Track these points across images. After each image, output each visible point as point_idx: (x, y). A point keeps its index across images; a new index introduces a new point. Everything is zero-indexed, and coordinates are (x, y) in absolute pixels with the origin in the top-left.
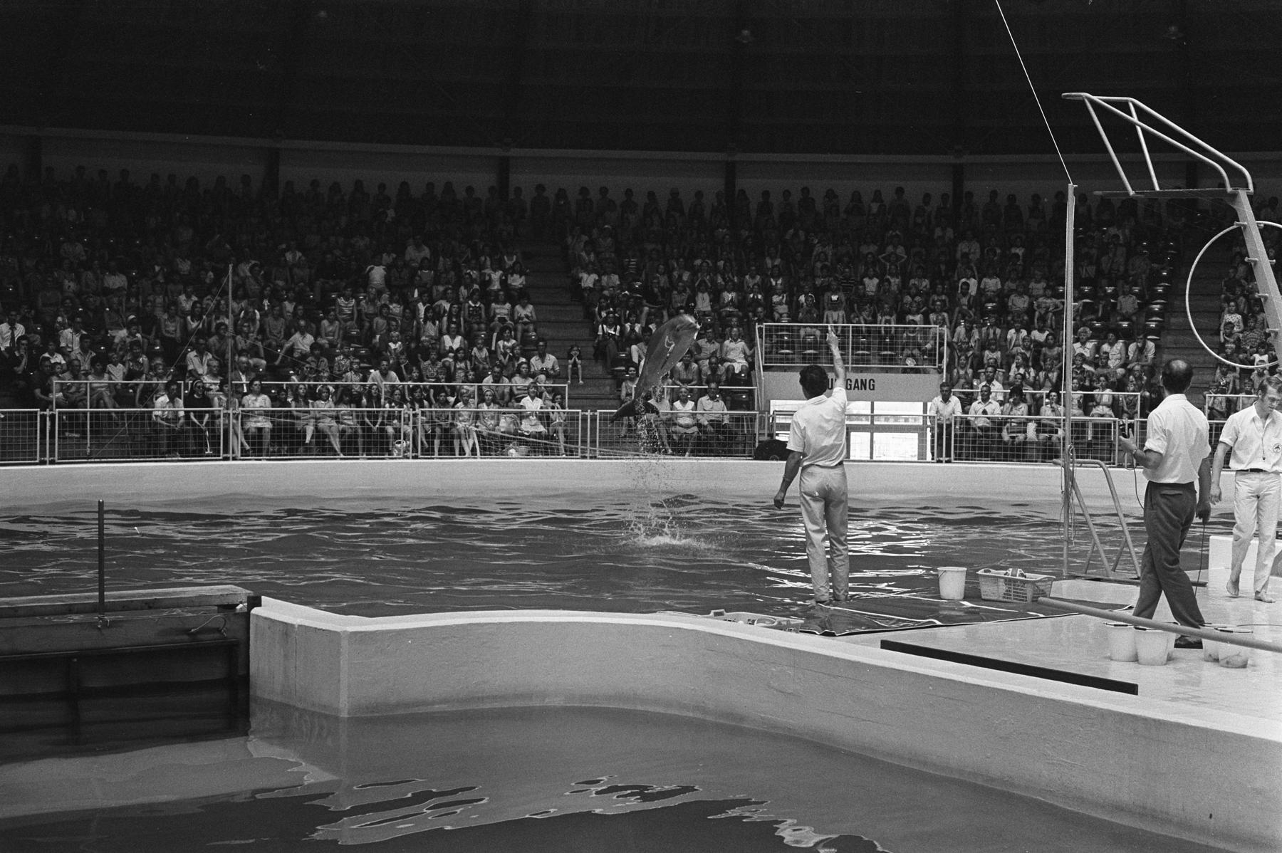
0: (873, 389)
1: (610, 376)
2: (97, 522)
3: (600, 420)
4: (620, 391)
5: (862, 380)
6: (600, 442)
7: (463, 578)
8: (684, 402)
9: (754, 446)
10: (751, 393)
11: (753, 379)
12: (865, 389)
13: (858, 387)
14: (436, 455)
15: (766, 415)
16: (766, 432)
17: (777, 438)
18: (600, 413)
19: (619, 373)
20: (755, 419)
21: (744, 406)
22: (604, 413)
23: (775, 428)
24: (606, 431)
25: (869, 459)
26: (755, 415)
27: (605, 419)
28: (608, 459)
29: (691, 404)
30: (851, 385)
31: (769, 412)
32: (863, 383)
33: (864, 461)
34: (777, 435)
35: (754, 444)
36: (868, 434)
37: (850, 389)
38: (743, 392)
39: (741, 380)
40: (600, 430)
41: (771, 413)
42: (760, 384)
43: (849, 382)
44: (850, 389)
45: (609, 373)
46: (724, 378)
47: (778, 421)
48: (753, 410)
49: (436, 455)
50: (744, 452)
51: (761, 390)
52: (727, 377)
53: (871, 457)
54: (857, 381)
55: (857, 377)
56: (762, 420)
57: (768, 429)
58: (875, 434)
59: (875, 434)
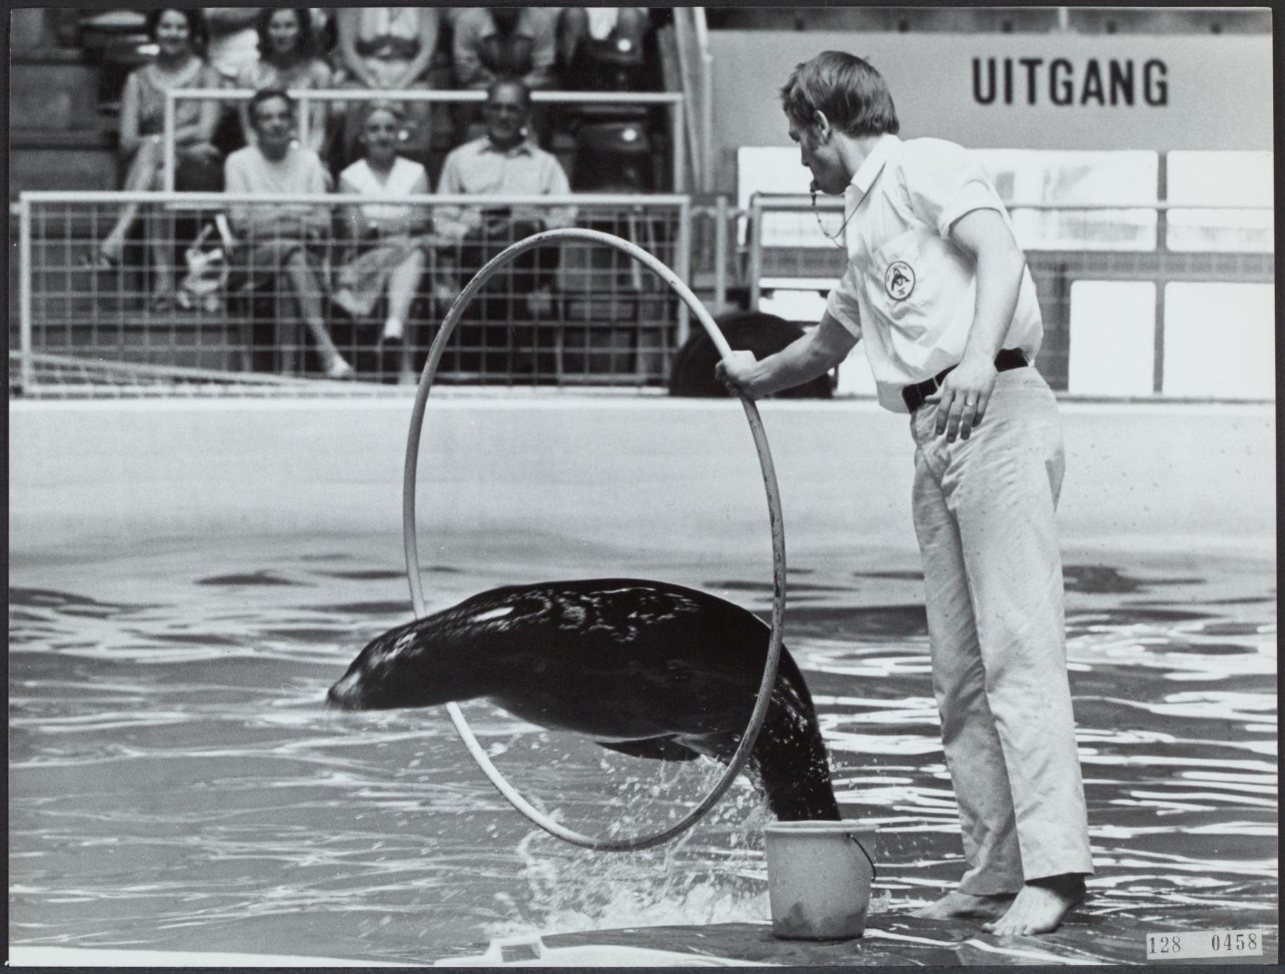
0: (1163, 100)
1: (72, 53)
2: (771, 595)
3: (34, 235)
4: (116, 114)
5: (1114, 66)
6: (35, 329)
7: (911, 890)
8: (383, 166)
9: (672, 340)
10: (657, 119)
11: (667, 63)
12: (1130, 99)
13: (1099, 94)
14: (613, 358)
15: (719, 212)
16: (721, 280)
17: (765, 306)
18: (35, 206)
19: (110, 42)
20: (676, 225)
21: (631, 173)
22: (49, 206)
23: (756, 265)
24: (56, 281)
25: (1147, 390)
26: (675, 211)
27: (55, 232)
28: (72, 396)
29: (408, 173)
30: (1068, 85)
31: (733, 199)
32: (1122, 80)
33: (1134, 400)
34: (766, 292)
35: (672, 331)
36: (1148, 289)
37: (1069, 100)
38: (625, 115)
39: (617, 67)
40: (35, 277)
41: (743, 203)
42: (696, 79)
43: (1061, 71)
44: (1069, 100)
45: (64, 42)
46: (546, 56)
47: (767, 239)
48: (668, 188)
49: (613, 358)
50: (629, 365)
51: (697, 103)
52: (559, 56)
53: (1158, 386)
54: (1093, 68)
55: (1093, 55)
56: (702, 227)
57: (730, 269)
58: (1172, 289)
59: (1172, 289)
